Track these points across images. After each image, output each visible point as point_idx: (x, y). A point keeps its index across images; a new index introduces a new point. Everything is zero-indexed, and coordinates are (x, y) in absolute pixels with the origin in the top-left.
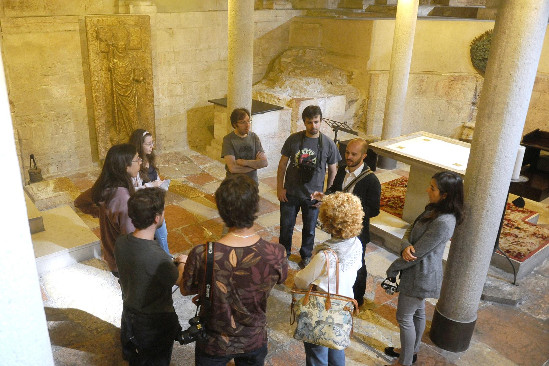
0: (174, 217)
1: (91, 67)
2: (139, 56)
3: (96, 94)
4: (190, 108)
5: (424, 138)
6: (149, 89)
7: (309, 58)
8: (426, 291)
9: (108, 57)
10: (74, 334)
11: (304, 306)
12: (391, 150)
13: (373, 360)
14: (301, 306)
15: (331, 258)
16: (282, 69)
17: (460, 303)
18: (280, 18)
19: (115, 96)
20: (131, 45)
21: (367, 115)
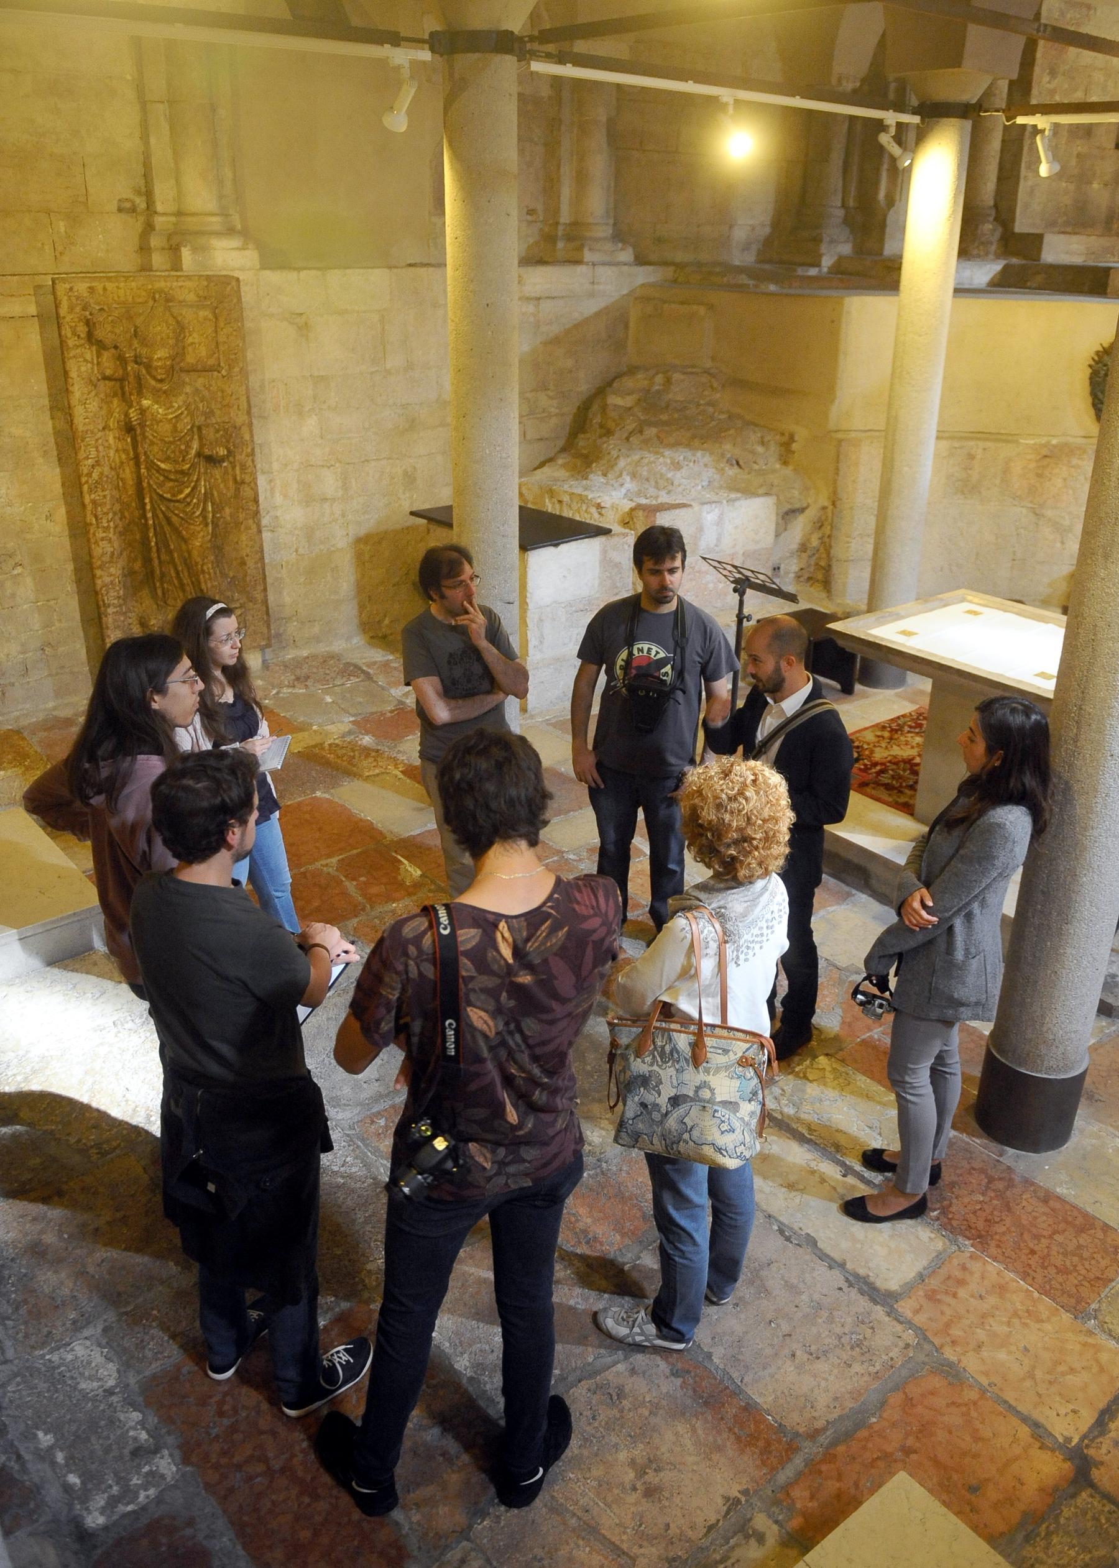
0: (320, 829)
1: (75, 421)
2: (214, 388)
3: (93, 496)
4: (362, 532)
5: (966, 606)
6: (243, 482)
7: (679, 398)
8: (962, 1005)
9: (123, 394)
10: (35, 1161)
11: (639, 1060)
12: (882, 639)
13: (833, 1184)
14: (632, 1058)
15: (706, 932)
16: (611, 424)
17: (1045, 1029)
18: (601, 287)
19: (147, 500)
20: (190, 359)
21: (830, 547)
